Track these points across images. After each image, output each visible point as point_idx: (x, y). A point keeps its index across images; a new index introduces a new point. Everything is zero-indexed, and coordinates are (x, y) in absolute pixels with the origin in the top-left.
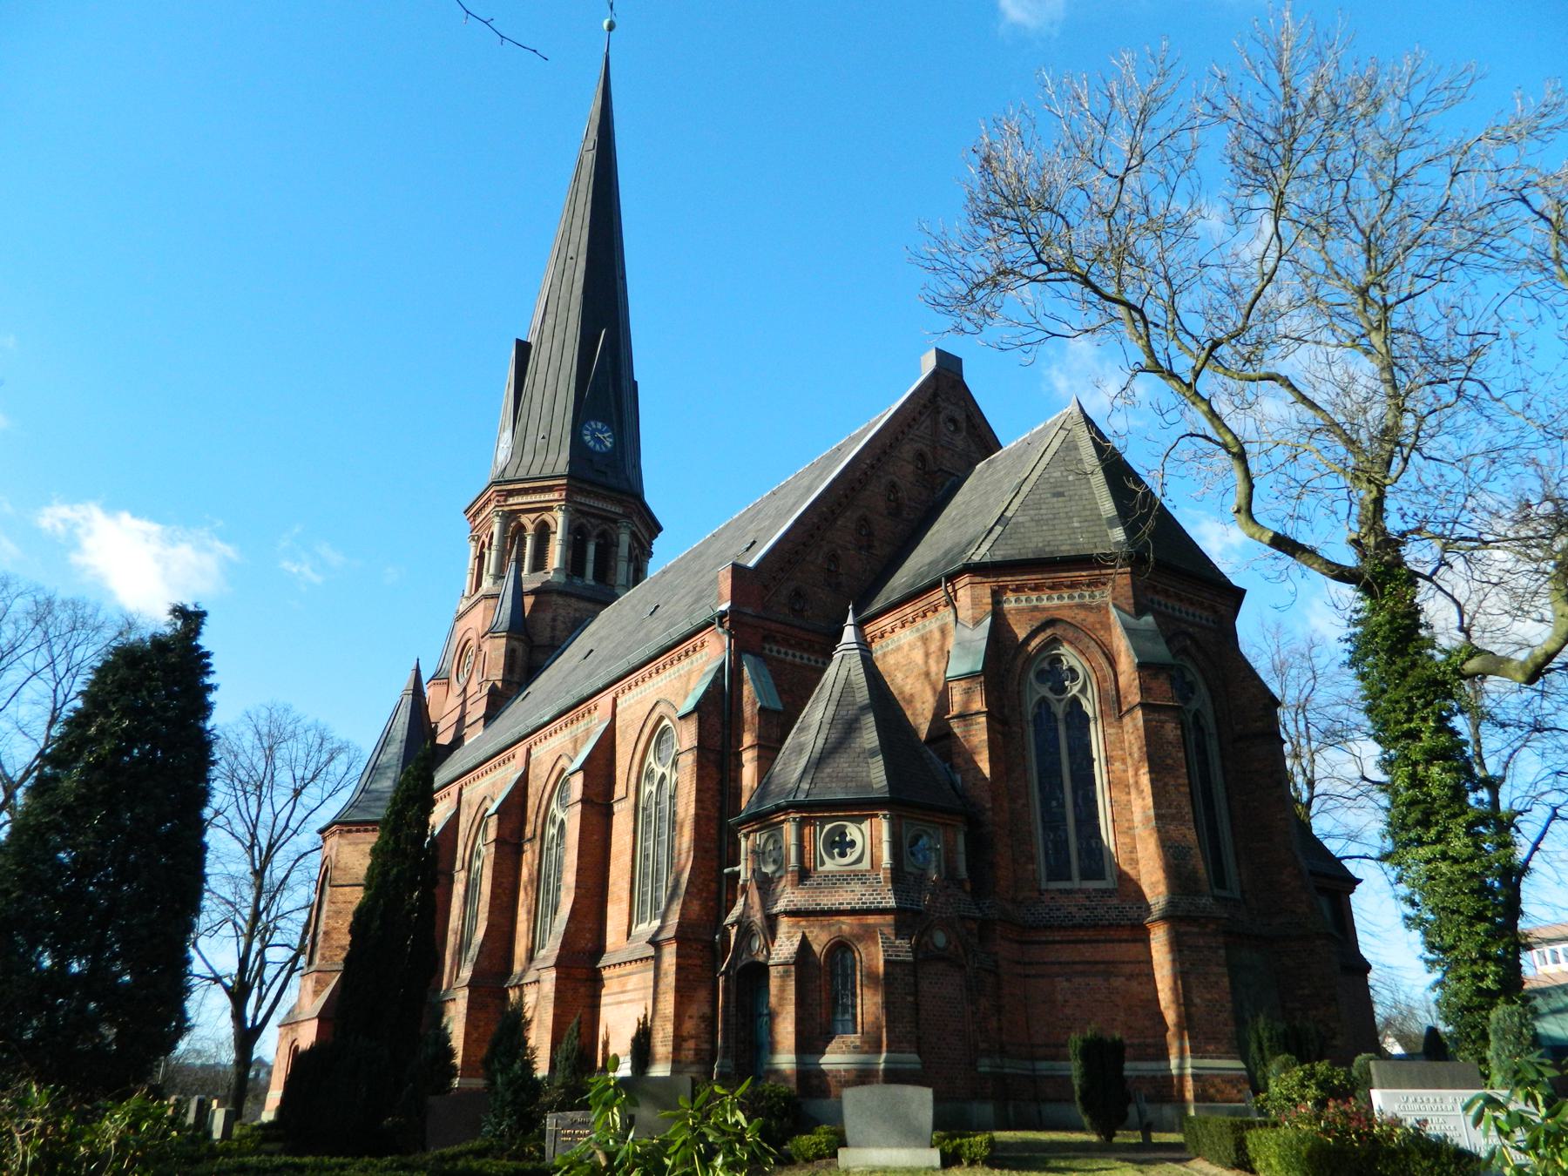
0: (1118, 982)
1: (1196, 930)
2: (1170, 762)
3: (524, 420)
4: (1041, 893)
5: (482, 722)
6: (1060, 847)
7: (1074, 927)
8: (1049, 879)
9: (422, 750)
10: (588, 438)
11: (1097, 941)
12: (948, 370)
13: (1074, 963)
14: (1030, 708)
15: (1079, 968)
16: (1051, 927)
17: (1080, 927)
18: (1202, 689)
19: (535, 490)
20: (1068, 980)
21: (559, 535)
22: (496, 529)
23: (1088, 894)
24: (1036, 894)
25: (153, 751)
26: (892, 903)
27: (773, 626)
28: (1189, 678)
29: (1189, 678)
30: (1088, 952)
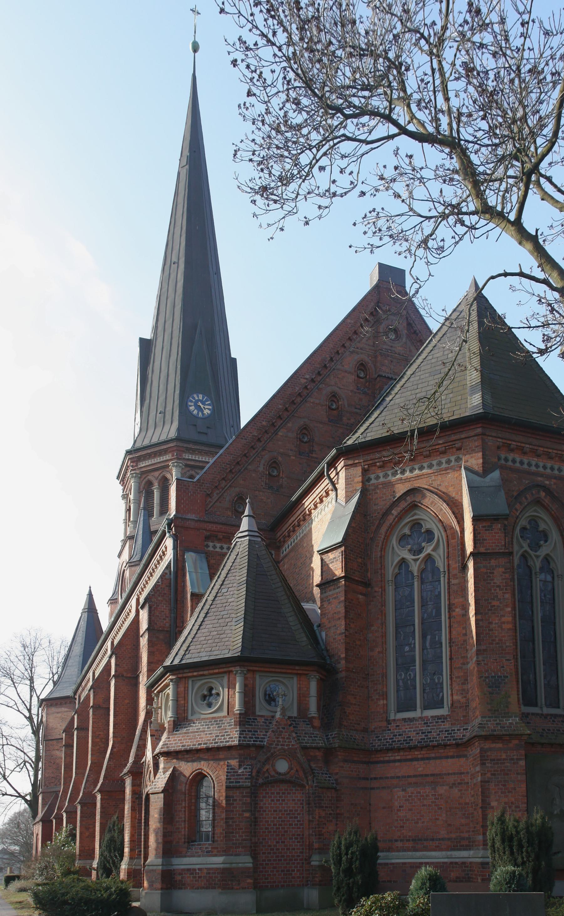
0: (442, 790)
1: (500, 745)
2: (495, 603)
3: (147, 402)
4: (389, 722)
6: (409, 687)
7: (411, 748)
8: (399, 710)
10: (192, 408)
11: (428, 759)
12: (391, 278)
13: (409, 777)
14: (391, 571)
15: (413, 780)
16: (392, 750)
17: (415, 748)
18: (555, 536)
20: (404, 790)
23: (425, 721)
24: (384, 724)
27: (214, 527)
28: (542, 526)
29: (542, 526)
30: (420, 767)
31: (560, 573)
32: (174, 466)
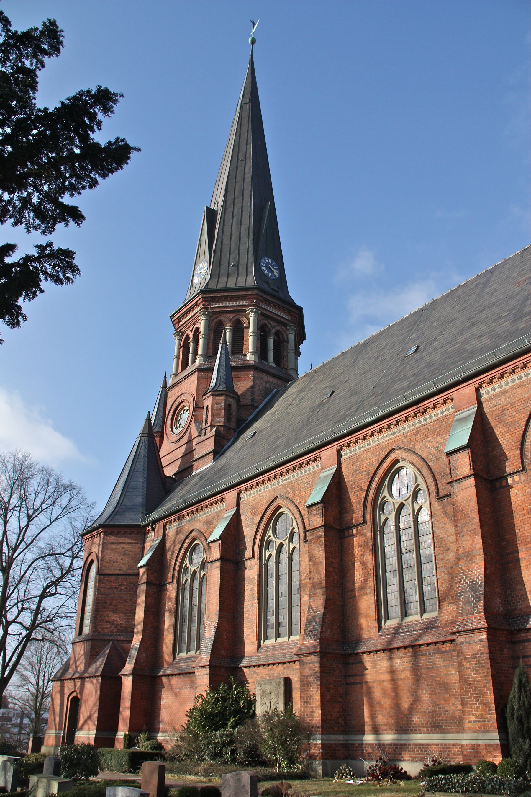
5: (211, 456)
9: (151, 484)
10: (264, 268)
19: (231, 298)
21: (251, 329)
22: (202, 325)
25: (46, 130)
26: (486, 625)
31: (178, 338)
32: (252, 311)
